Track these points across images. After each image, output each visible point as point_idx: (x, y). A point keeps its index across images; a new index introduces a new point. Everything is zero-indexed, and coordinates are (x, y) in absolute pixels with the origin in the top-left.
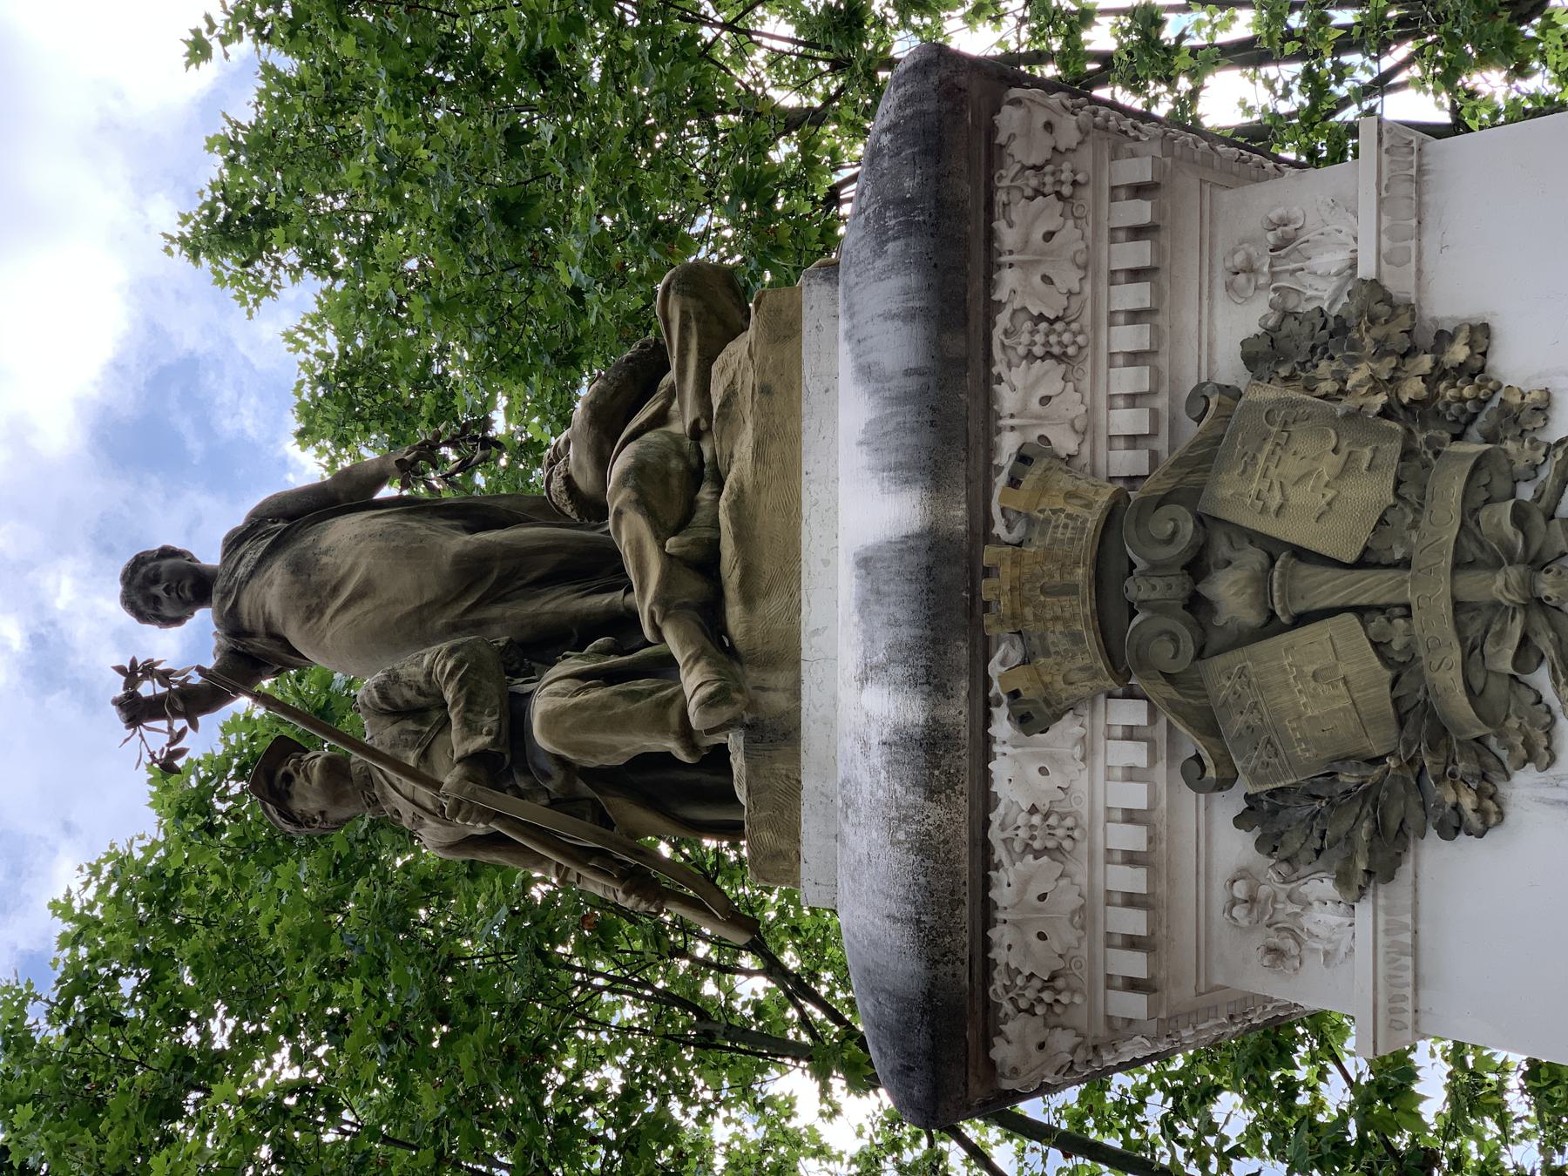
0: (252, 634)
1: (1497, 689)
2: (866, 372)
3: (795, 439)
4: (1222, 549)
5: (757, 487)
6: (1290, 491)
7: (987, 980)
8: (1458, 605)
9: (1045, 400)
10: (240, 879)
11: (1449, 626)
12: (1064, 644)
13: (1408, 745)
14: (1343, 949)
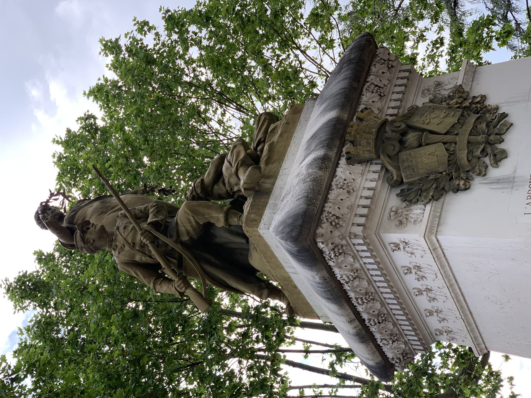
6: (431, 120)
7: (321, 214)
8: (469, 142)
9: (373, 102)
11: (465, 146)
12: (365, 144)
13: (449, 170)
14: (419, 220)
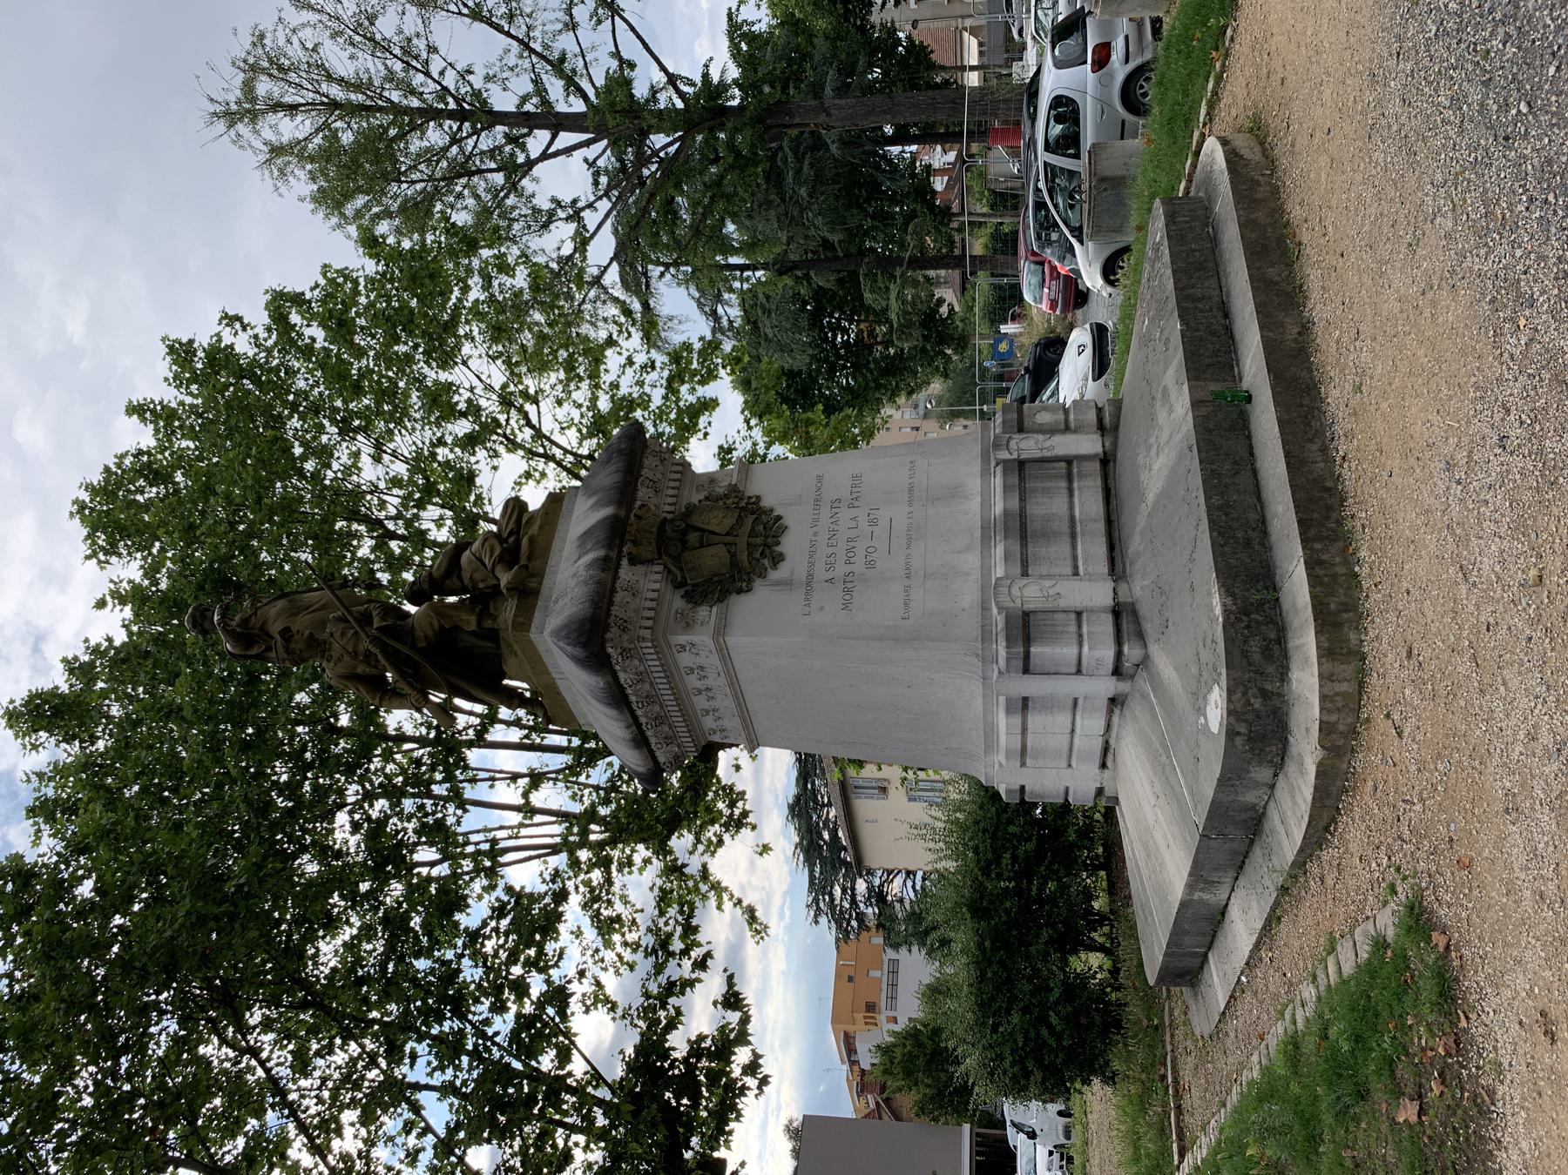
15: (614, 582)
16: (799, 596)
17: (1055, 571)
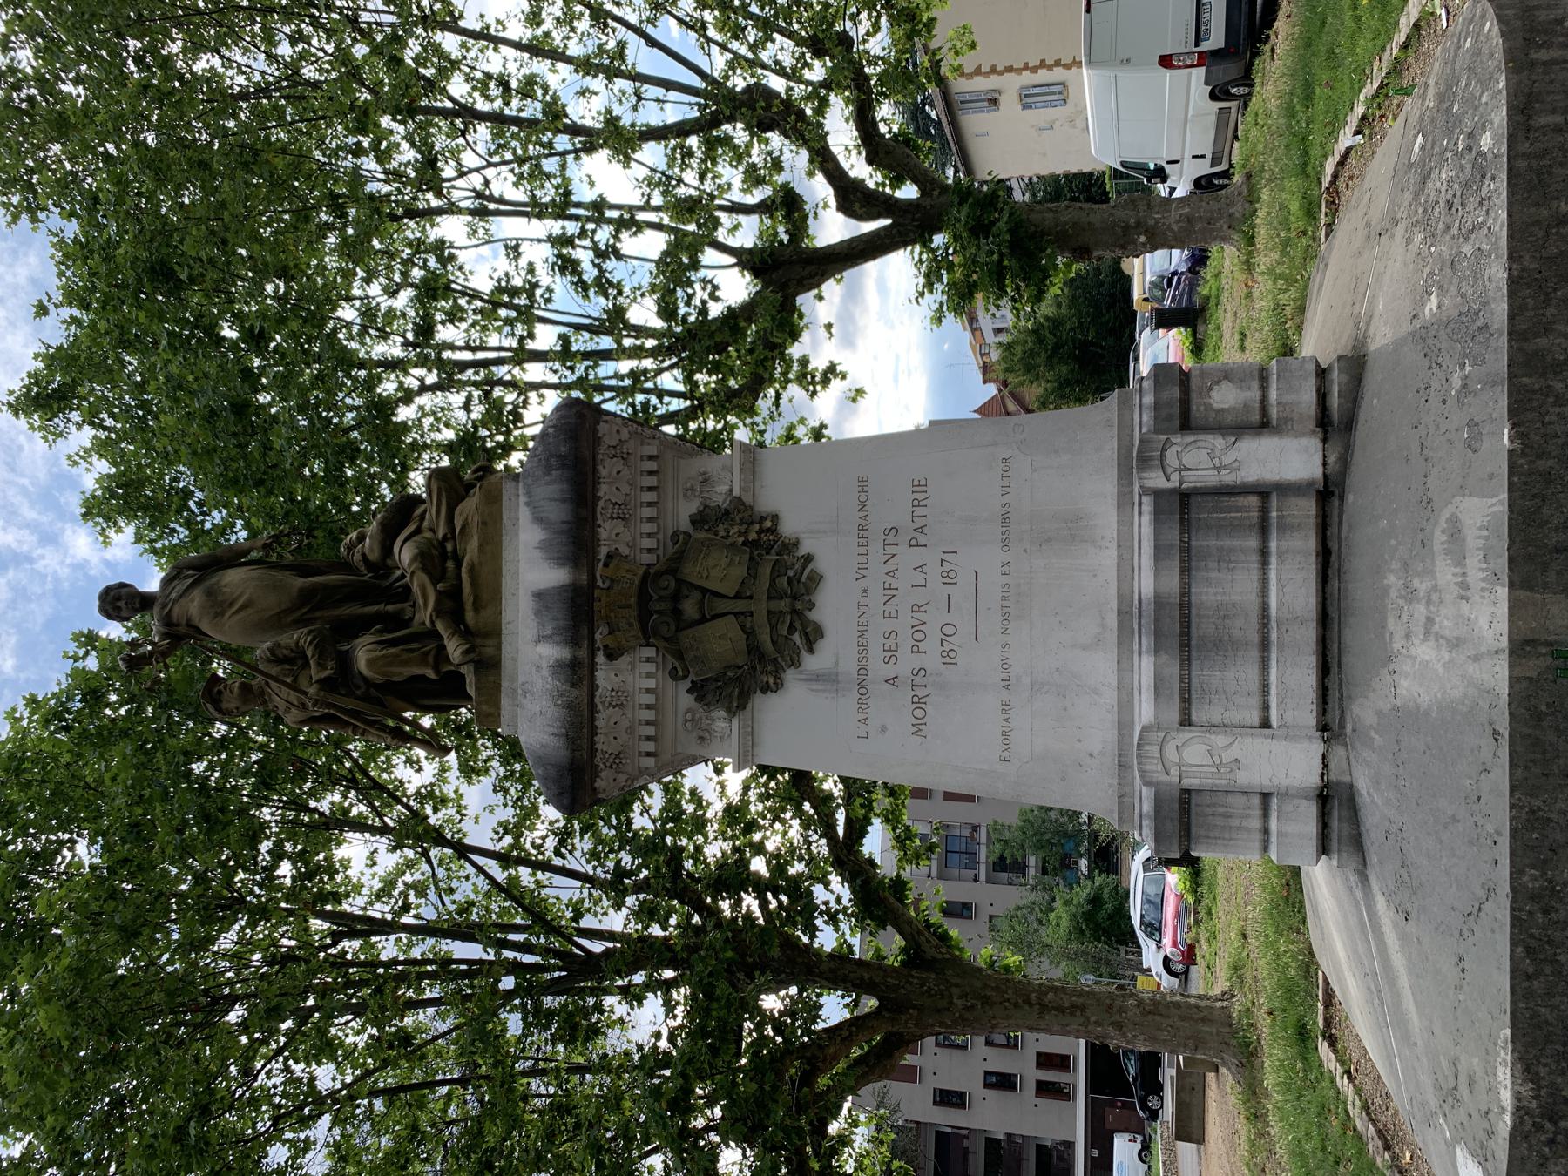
0: (178, 625)
1: (781, 641)
2: (539, 520)
3: (499, 544)
4: (685, 592)
5: (480, 564)
8: (769, 612)
10: (80, 756)
15: (592, 696)
16: (850, 700)
17: (1233, 716)
